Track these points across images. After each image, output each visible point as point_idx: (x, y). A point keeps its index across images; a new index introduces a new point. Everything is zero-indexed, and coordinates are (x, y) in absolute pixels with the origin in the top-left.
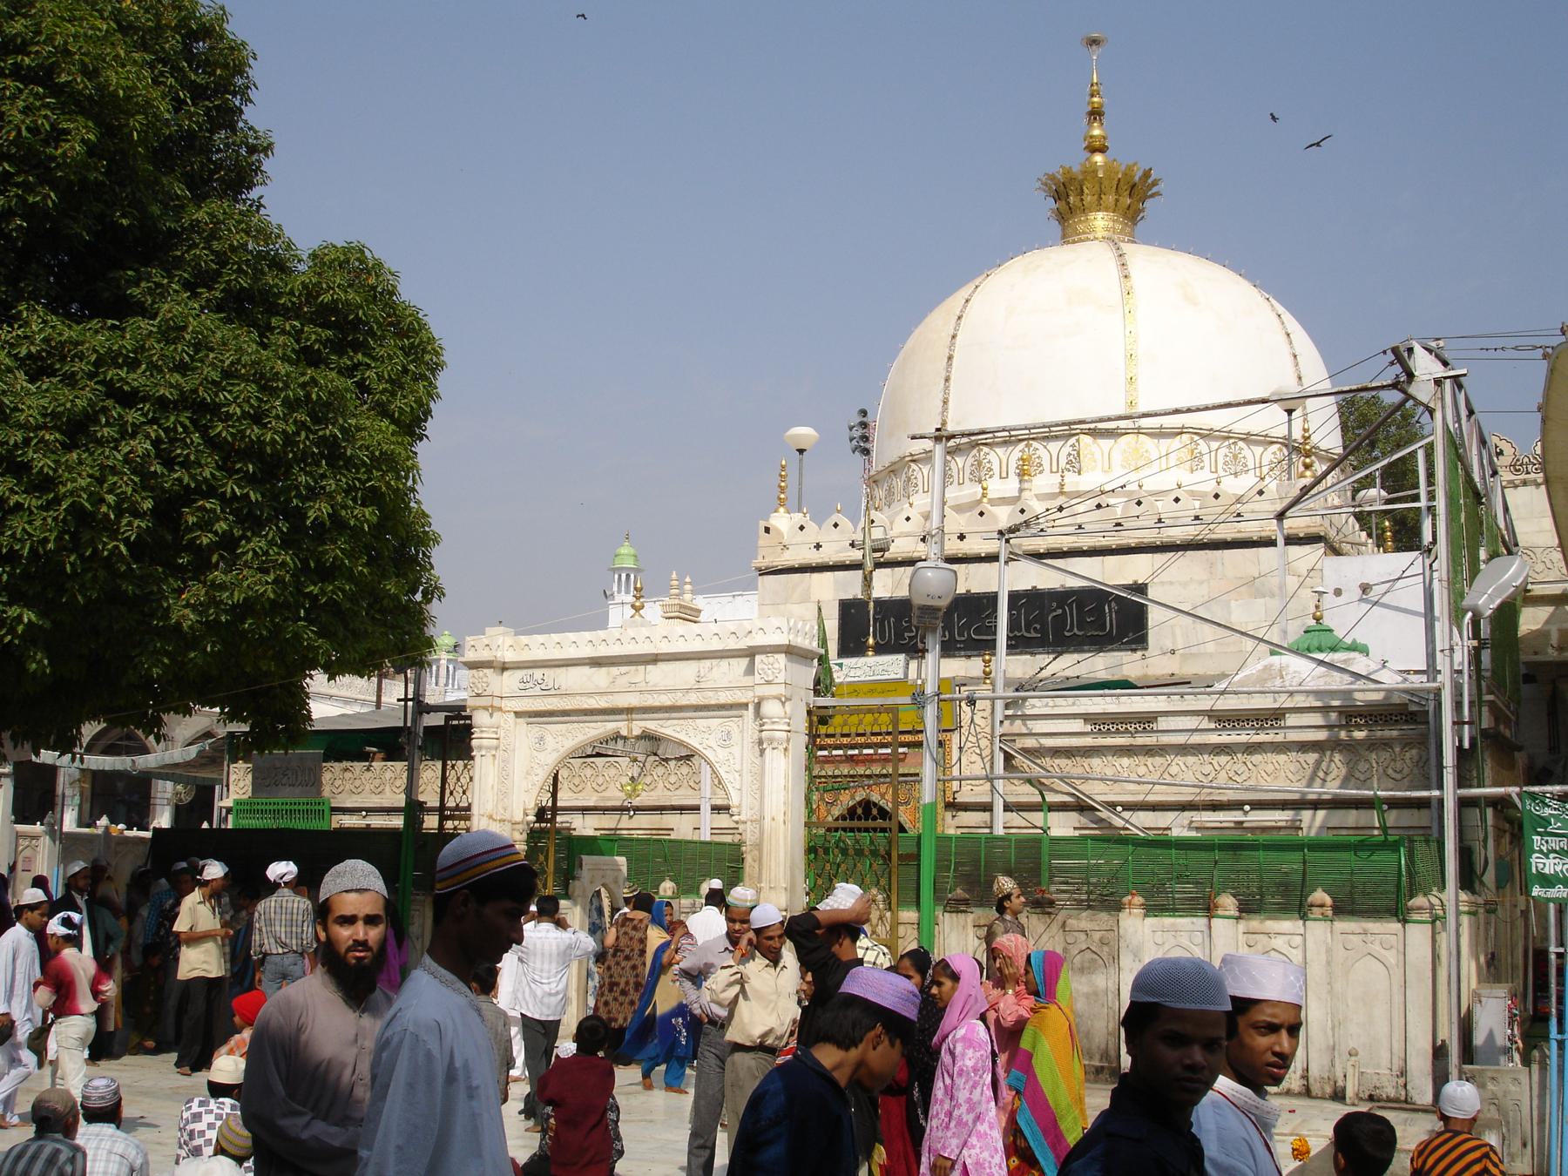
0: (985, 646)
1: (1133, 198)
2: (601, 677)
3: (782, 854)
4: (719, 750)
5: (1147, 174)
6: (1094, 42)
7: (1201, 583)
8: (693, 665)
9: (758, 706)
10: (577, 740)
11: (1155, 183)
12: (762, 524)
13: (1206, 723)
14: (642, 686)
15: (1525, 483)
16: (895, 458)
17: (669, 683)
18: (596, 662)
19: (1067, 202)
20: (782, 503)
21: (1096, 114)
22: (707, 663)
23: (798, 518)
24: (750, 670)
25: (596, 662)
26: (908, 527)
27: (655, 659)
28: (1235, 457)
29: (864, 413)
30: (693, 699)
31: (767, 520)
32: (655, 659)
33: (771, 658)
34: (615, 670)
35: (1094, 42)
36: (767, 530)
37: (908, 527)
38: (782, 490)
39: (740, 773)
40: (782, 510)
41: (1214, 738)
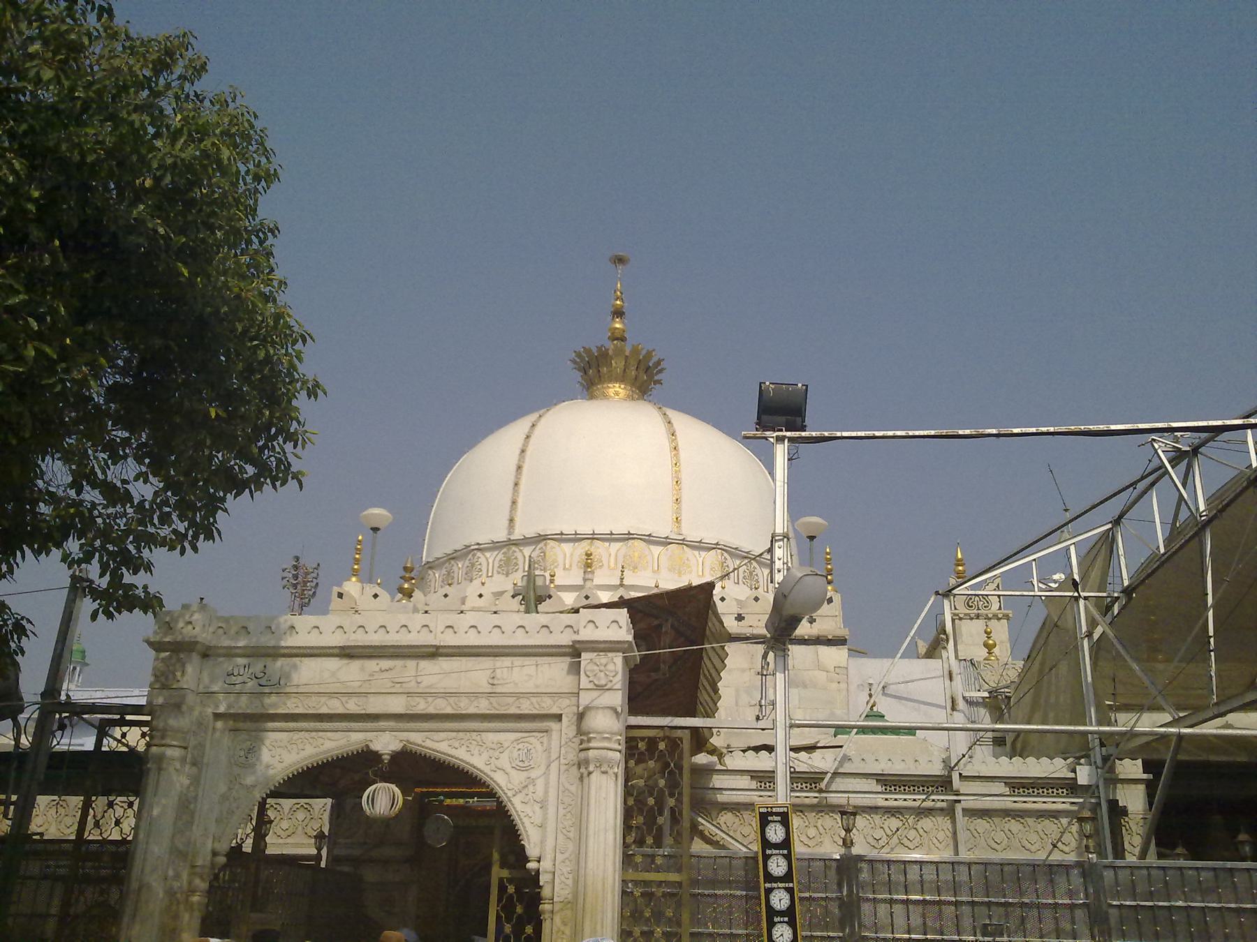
0: (638, 699)
1: (645, 380)
2: (352, 672)
3: (609, 915)
4: (513, 773)
5: (658, 363)
6: (620, 260)
7: (743, 671)
8: (487, 662)
9: (581, 716)
10: (303, 754)
11: (660, 371)
12: (336, 590)
13: (872, 785)
14: (412, 686)
15: (978, 617)
16: (459, 546)
17: (450, 684)
18: (347, 653)
19: (592, 373)
20: (355, 573)
21: (618, 313)
22: (507, 661)
23: (371, 589)
24: (575, 669)
25: (347, 653)
26: (480, 603)
27: (434, 653)
28: (751, 573)
29: (297, 559)
30: (483, 707)
31: (340, 585)
32: (434, 653)
33: (602, 659)
34: (372, 665)
35: (620, 260)
36: (340, 595)
37: (480, 603)
38: (357, 561)
39: (543, 804)
40: (354, 579)
41: (880, 800)
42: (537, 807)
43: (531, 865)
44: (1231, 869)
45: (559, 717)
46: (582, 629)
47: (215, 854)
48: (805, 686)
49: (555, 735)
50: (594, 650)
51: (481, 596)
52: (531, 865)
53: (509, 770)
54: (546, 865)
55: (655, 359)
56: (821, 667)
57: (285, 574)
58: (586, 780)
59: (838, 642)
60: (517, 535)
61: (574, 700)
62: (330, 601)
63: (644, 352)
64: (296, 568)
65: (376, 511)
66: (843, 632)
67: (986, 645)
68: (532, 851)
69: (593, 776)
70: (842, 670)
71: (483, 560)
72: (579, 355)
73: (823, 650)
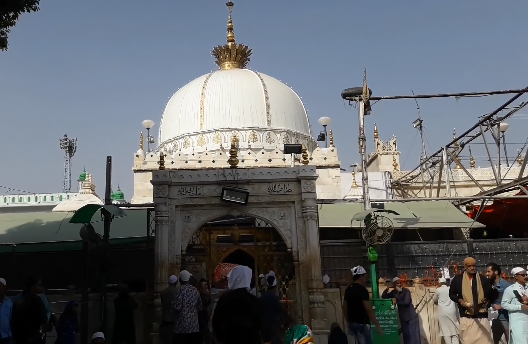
1: (241, 58)
5: (250, 51)
11: (250, 55)
12: (135, 154)
15: (387, 154)
29: (66, 136)
30: (267, 199)
35: (230, 5)
36: (137, 156)
42: (289, 232)
43: (289, 250)
44: (156, 221)
45: (294, 202)
46: (300, 172)
47: (182, 251)
48: (324, 185)
49: (293, 208)
50: (305, 179)
51: (193, 155)
52: (289, 250)
53: (278, 220)
54: (294, 249)
55: (248, 50)
56: (329, 177)
57: (62, 142)
58: (306, 223)
59: (336, 167)
60: (204, 130)
61: (298, 196)
62: (134, 158)
63: (244, 47)
64: (66, 140)
65: (146, 121)
66: (338, 163)
67: (393, 165)
68: (288, 244)
69: (309, 221)
70: (337, 177)
71: (190, 140)
72: (216, 49)
73: (330, 170)
